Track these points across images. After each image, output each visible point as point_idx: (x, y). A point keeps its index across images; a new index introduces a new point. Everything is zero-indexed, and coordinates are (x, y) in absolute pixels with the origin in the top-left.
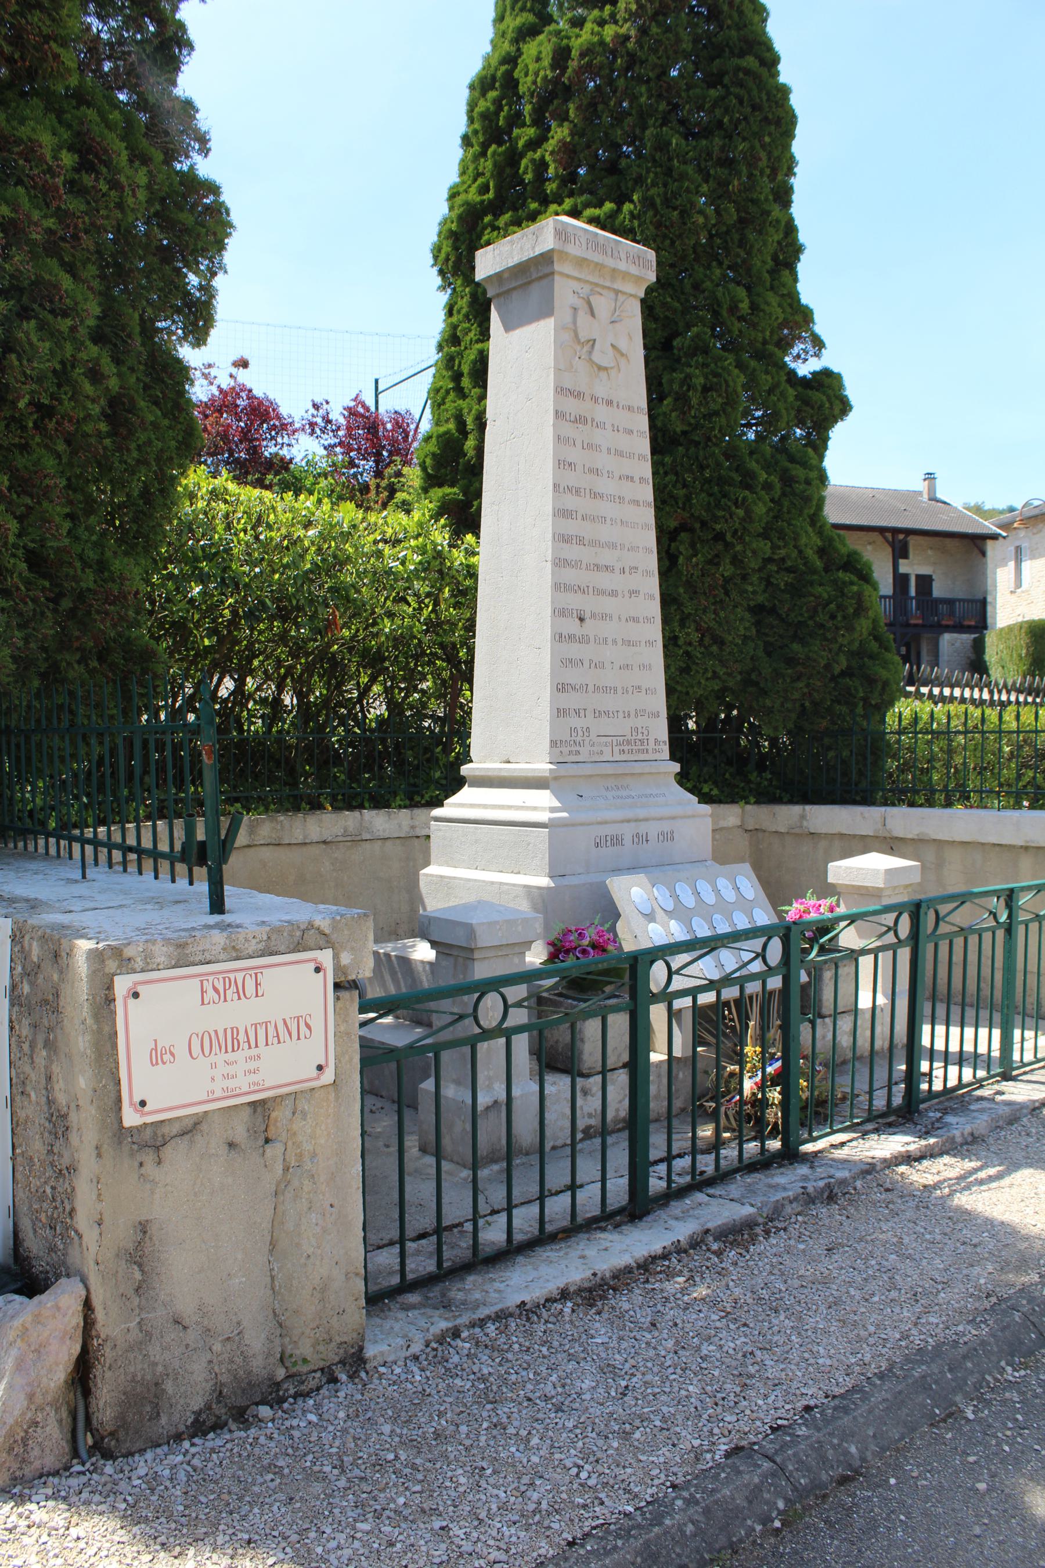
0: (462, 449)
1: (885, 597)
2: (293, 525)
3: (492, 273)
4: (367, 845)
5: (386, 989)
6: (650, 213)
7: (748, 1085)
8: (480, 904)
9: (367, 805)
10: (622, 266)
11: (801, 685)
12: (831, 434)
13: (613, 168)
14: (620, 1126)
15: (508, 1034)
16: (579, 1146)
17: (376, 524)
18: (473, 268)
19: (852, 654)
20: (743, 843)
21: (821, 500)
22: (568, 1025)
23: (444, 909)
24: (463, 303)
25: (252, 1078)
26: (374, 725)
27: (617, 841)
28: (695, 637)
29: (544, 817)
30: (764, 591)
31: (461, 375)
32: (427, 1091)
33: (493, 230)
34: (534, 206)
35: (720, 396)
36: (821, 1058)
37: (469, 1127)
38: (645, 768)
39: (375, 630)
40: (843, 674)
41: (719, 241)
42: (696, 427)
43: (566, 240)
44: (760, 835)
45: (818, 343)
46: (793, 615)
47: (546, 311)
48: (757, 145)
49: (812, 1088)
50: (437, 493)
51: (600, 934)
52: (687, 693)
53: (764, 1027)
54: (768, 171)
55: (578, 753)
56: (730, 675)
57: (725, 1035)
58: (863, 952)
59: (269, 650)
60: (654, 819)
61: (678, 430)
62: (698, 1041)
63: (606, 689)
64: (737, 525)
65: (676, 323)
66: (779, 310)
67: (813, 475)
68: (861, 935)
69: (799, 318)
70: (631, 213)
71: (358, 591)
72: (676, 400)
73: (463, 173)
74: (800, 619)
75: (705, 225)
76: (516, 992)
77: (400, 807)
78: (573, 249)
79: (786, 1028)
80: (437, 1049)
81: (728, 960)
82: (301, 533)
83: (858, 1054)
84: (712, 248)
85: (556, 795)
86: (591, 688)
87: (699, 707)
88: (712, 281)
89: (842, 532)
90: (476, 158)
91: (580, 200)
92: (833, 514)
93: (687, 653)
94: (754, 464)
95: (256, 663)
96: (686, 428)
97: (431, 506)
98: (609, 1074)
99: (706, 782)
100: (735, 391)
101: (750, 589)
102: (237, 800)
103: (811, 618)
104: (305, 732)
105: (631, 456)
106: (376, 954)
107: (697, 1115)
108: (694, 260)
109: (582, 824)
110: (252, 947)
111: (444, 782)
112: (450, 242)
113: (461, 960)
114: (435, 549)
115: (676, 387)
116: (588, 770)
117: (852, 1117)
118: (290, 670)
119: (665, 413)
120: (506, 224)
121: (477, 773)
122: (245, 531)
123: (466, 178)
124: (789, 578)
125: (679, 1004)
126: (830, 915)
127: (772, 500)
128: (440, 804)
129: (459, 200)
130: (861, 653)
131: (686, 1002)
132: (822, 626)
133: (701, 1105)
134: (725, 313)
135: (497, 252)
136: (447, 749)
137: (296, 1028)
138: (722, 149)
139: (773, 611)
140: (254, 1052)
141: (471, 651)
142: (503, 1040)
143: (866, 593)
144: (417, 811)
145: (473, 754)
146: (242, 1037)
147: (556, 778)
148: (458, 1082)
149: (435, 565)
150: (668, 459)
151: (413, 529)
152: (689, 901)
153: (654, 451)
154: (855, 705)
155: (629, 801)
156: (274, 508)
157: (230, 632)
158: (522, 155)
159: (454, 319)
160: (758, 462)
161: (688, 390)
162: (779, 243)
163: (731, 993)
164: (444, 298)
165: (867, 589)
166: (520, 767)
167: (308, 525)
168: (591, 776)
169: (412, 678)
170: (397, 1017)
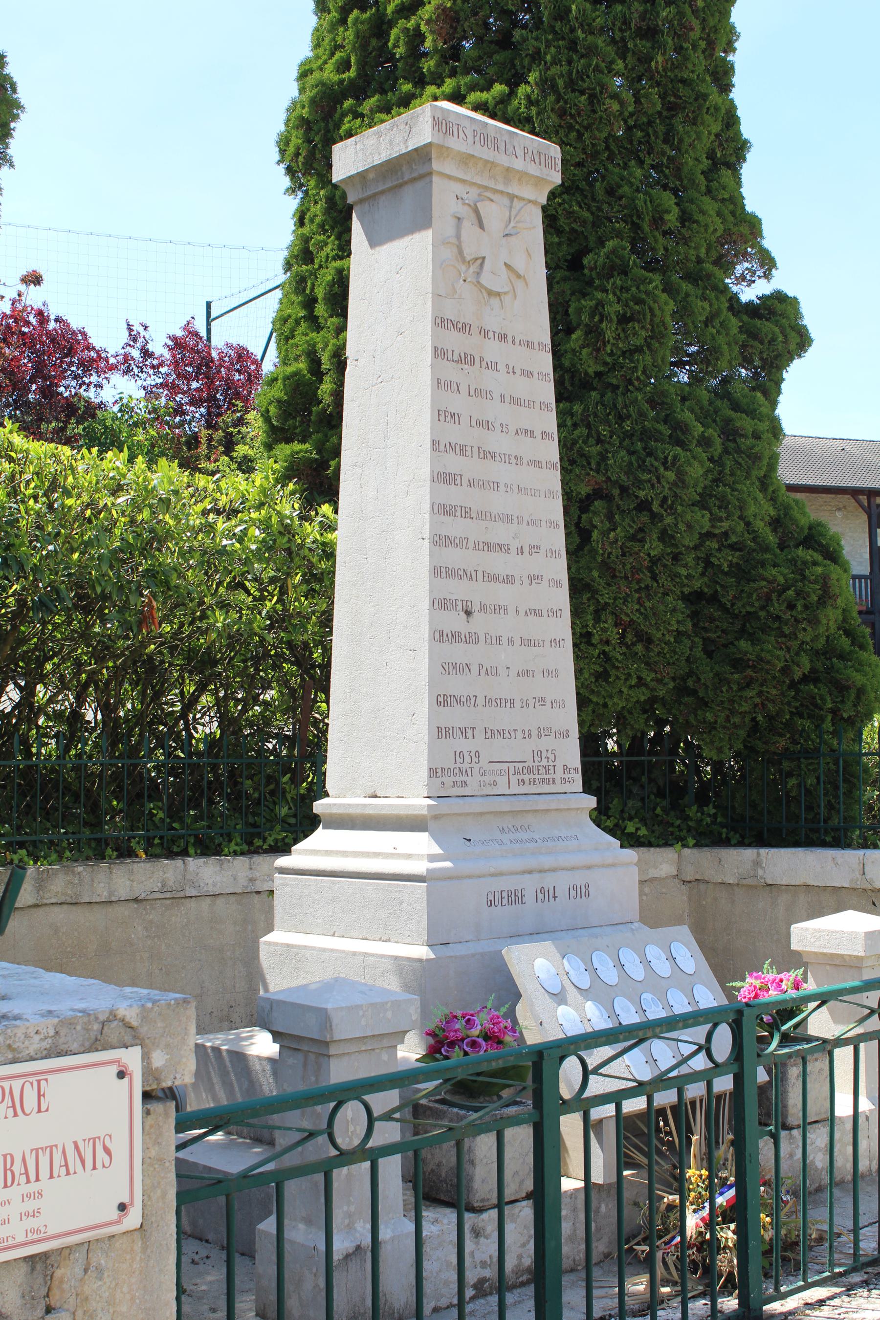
0: (315, 394)
1: (860, 577)
2: (98, 491)
4: (192, 903)
5: (215, 1098)
6: (552, 98)
7: (693, 1222)
8: (336, 984)
9: (191, 851)
10: (519, 164)
11: (750, 693)
12: (785, 375)
13: (505, 42)
14: (524, 1278)
15: (374, 1156)
16: (469, 1308)
17: (205, 489)
18: (330, 166)
19: (816, 654)
20: (679, 897)
21: (774, 459)
22: (453, 1142)
23: (289, 990)
24: (317, 210)
25: (32, 1223)
26: (201, 746)
27: (516, 897)
28: (614, 634)
29: (420, 867)
30: (703, 574)
31: (315, 300)
32: (267, 1234)
33: (355, 117)
34: (407, 87)
35: (643, 327)
36: (787, 1184)
37: (322, 1283)
39: (204, 625)
40: (805, 679)
41: (639, 134)
42: (613, 368)
43: (448, 132)
44: (702, 887)
45: (768, 263)
46: (739, 604)
47: (422, 220)
48: (688, 11)
49: (777, 1225)
50: (284, 450)
51: (495, 1021)
52: (605, 705)
53: (712, 1142)
54: (703, 44)
56: (659, 681)
57: (660, 1153)
58: (840, 1042)
59: (66, 650)
61: (591, 371)
62: (623, 1161)
63: (500, 702)
64: (666, 492)
65: (586, 238)
66: (718, 221)
67: (764, 426)
68: (836, 1019)
69: (745, 229)
70: (528, 97)
71: (182, 576)
72: (587, 333)
73: (317, 46)
74: (749, 609)
76: (385, 1100)
77: (235, 854)
78: (455, 143)
79: (739, 1144)
80: (279, 1179)
81: (663, 1053)
82: (109, 501)
83: (838, 1177)
84: (631, 142)
86: (480, 701)
87: (621, 721)
89: (799, 496)
90: (333, 28)
91: (465, 80)
92: (788, 473)
93: (604, 653)
94: (687, 413)
95: (49, 667)
97: (276, 466)
98: (507, 1209)
99: (631, 819)
100: (664, 323)
101: (683, 572)
102: (22, 845)
103: (763, 608)
104: (112, 757)
105: (530, 404)
106: (200, 1049)
107: (625, 1260)
109: (470, 877)
110: (35, 1045)
111: (292, 821)
112: (301, 132)
113: (312, 1057)
114: (281, 522)
115: (585, 318)
116: (477, 805)
117: (832, 1265)
118: (92, 674)
119: (573, 350)
120: (371, 110)
121: (335, 811)
122: (35, 498)
123: (320, 51)
124: (734, 557)
125: (597, 1113)
126: (792, 994)
127: (711, 459)
128: (284, 849)
129: (311, 80)
130: (829, 651)
131: (609, 1110)
132: (778, 618)
133: (631, 1249)
136: (297, 777)
137: (92, 1153)
138: (643, 17)
139: (714, 599)
140: (34, 1187)
141: (327, 651)
142: (368, 1164)
143: (834, 576)
144: (257, 859)
145: (329, 787)
146: (18, 1168)
147: (436, 817)
148: (308, 1221)
149: (282, 544)
150: (577, 408)
151: (253, 496)
152: (610, 975)
153: (560, 398)
154: (822, 719)
156: (73, 469)
157: (15, 628)
158: (391, 24)
159: (306, 230)
160: (692, 411)
161: (601, 321)
162: (717, 135)
163: (666, 1098)
164: (293, 203)
165: (835, 571)
166: (389, 804)
167: (117, 489)
168: (481, 814)
169: (254, 685)
170: (229, 1133)
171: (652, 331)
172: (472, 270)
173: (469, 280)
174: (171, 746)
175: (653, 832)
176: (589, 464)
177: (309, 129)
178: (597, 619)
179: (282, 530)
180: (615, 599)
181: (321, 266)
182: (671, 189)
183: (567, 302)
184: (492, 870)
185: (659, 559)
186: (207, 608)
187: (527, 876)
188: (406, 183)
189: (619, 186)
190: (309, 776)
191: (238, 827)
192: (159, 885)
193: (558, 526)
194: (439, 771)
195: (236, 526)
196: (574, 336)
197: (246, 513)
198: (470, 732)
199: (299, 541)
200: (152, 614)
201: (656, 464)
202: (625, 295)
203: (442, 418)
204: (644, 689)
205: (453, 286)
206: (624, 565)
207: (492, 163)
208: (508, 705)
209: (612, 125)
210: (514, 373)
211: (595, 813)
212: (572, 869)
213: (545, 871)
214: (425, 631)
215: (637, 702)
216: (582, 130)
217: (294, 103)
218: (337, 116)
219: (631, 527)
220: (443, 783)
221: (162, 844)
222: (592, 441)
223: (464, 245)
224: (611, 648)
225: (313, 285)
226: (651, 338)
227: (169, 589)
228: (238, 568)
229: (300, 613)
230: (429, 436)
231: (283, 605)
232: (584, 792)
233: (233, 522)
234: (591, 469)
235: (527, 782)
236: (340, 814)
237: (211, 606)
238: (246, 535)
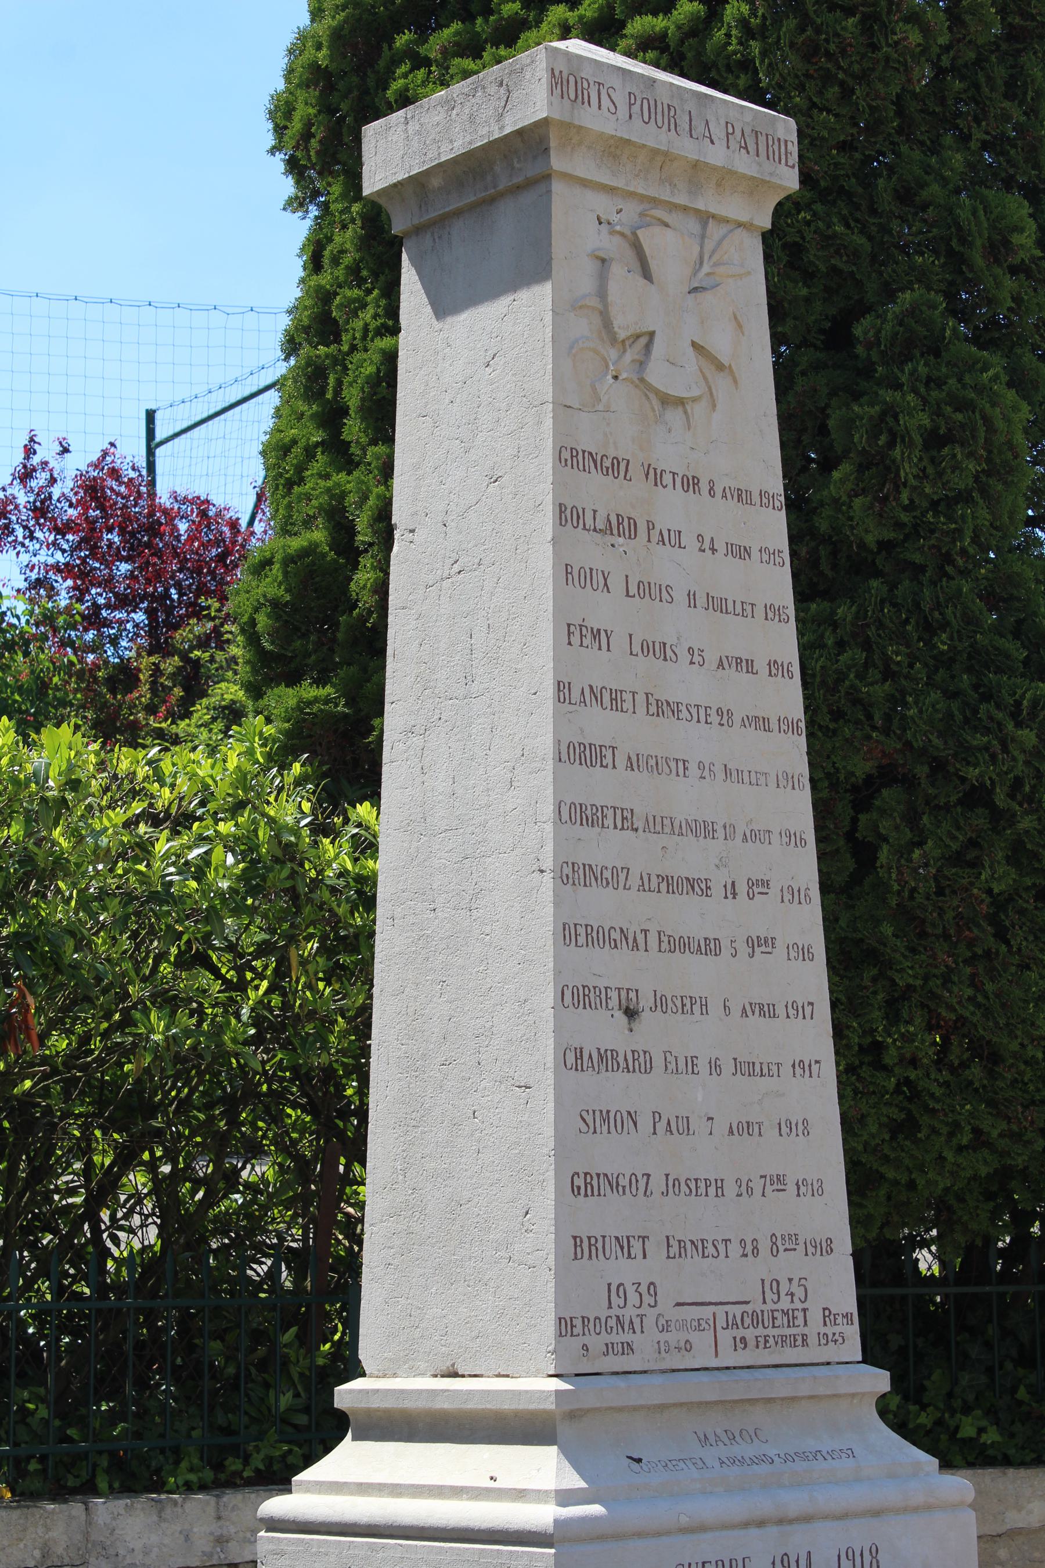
0: (345, 590)
3: (401, 176)
6: (790, 24)
9: (103, 1485)
10: (716, 155)
17: (132, 776)
24: (346, 239)
29: (542, 1515)
31: (344, 412)
33: (415, 68)
35: (971, 455)
38: (803, 1383)
43: (580, 98)
47: (533, 267)
50: (285, 698)
52: (912, 1185)
55: (628, 1348)
56: (1016, 1137)
60: (826, 1517)
61: (870, 539)
63: (696, 1186)
64: (1020, 768)
71: (82, 944)
72: (861, 468)
75: (925, 50)
77: (189, 1488)
78: (595, 120)
84: (942, 101)
85: (573, 1457)
86: (657, 1183)
87: (945, 1215)
88: (944, 181)
93: (907, 1082)
96: (889, 535)
97: (269, 730)
99: (967, 1410)
100: (1011, 446)
105: (746, 610)
108: (900, 131)
109: (640, 1535)
111: (302, 1420)
115: (860, 439)
116: (653, 1391)
119: (836, 501)
120: (444, 51)
121: (376, 1404)
128: (279, 1478)
134: (979, 260)
135: (413, 126)
136: (312, 1331)
144: (232, 1498)
145: (365, 1353)
147: (573, 1415)
149: (276, 876)
150: (844, 611)
155: (763, 1469)
159: (325, 279)
161: (891, 444)
164: (299, 228)
168: (662, 1407)
171: (989, 460)
172: (629, 357)
173: (624, 375)
174: (67, 1275)
175: (1012, 1435)
176: (870, 717)
177: (329, 88)
178: (893, 1017)
179: (279, 853)
180: (926, 978)
181: (353, 348)
182: (1021, 187)
183: (823, 410)
184: (684, 1520)
185: (1010, 899)
186: (134, 1007)
187: (753, 1531)
188: (501, 195)
189: (922, 185)
190: (335, 1330)
191: (195, 1434)
192: (37, 1553)
193: (803, 842)
194: (578, 1322)
195: (190, 848)
196: (836, 475)
197: (209, 821)
198: (637, 1247)
199: (313, 874)
200: (25, 1020)
201: (1000, 715)
202: (935, 394)
203: (576, 639)
204: (986, 1152)
205: (594, 389)
206: (941, 912)
207: (666, 154)
208: (712, 1190)
209: (907, 70)
210: (713, 550)
211: (895, 1401)
212: (844, 1516)
213: (791, 1522)
214: (547, 1049)
215: (975, 1177)
216: (850, 81)
217: (303, 36)
218: (382, 64)
219: (954, 838)
220: (585, 1347)
221: (44, 1471)
222: (874, 674)
223: (614, 311)
224: (920, 1072)
225: (339, 383)
226: (988, 473)
227: (58, 970)
228: (189, 928)
229: (314, 1012)
230: (551, 675)
231: (284, 994)
232: (864, 1361)
233: (185, 839)
234: (874, 728)
235: (752, 1343)
236: (387, 1411)
237: (141, 1001)
238: (208, 864)
